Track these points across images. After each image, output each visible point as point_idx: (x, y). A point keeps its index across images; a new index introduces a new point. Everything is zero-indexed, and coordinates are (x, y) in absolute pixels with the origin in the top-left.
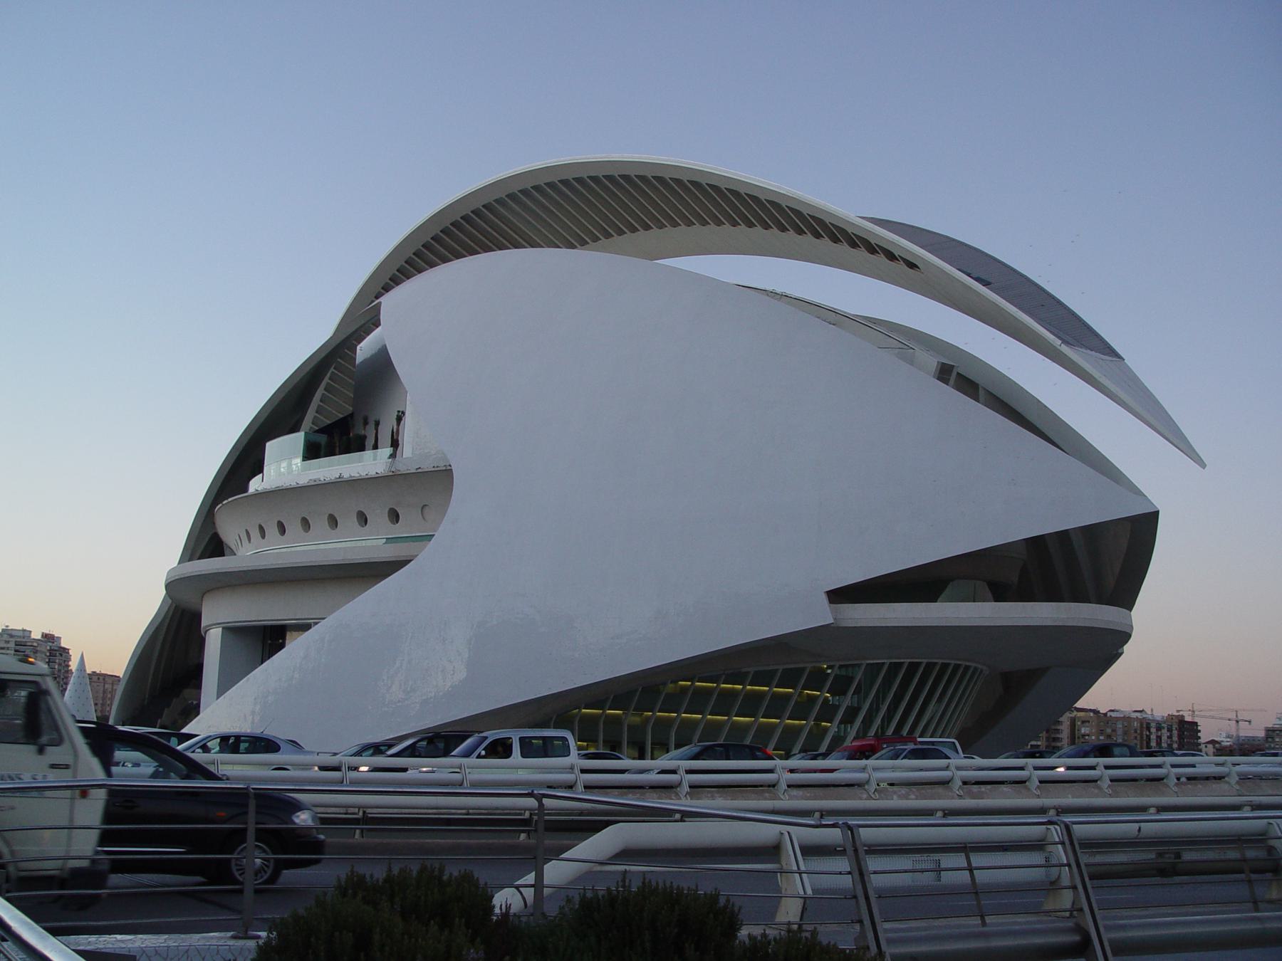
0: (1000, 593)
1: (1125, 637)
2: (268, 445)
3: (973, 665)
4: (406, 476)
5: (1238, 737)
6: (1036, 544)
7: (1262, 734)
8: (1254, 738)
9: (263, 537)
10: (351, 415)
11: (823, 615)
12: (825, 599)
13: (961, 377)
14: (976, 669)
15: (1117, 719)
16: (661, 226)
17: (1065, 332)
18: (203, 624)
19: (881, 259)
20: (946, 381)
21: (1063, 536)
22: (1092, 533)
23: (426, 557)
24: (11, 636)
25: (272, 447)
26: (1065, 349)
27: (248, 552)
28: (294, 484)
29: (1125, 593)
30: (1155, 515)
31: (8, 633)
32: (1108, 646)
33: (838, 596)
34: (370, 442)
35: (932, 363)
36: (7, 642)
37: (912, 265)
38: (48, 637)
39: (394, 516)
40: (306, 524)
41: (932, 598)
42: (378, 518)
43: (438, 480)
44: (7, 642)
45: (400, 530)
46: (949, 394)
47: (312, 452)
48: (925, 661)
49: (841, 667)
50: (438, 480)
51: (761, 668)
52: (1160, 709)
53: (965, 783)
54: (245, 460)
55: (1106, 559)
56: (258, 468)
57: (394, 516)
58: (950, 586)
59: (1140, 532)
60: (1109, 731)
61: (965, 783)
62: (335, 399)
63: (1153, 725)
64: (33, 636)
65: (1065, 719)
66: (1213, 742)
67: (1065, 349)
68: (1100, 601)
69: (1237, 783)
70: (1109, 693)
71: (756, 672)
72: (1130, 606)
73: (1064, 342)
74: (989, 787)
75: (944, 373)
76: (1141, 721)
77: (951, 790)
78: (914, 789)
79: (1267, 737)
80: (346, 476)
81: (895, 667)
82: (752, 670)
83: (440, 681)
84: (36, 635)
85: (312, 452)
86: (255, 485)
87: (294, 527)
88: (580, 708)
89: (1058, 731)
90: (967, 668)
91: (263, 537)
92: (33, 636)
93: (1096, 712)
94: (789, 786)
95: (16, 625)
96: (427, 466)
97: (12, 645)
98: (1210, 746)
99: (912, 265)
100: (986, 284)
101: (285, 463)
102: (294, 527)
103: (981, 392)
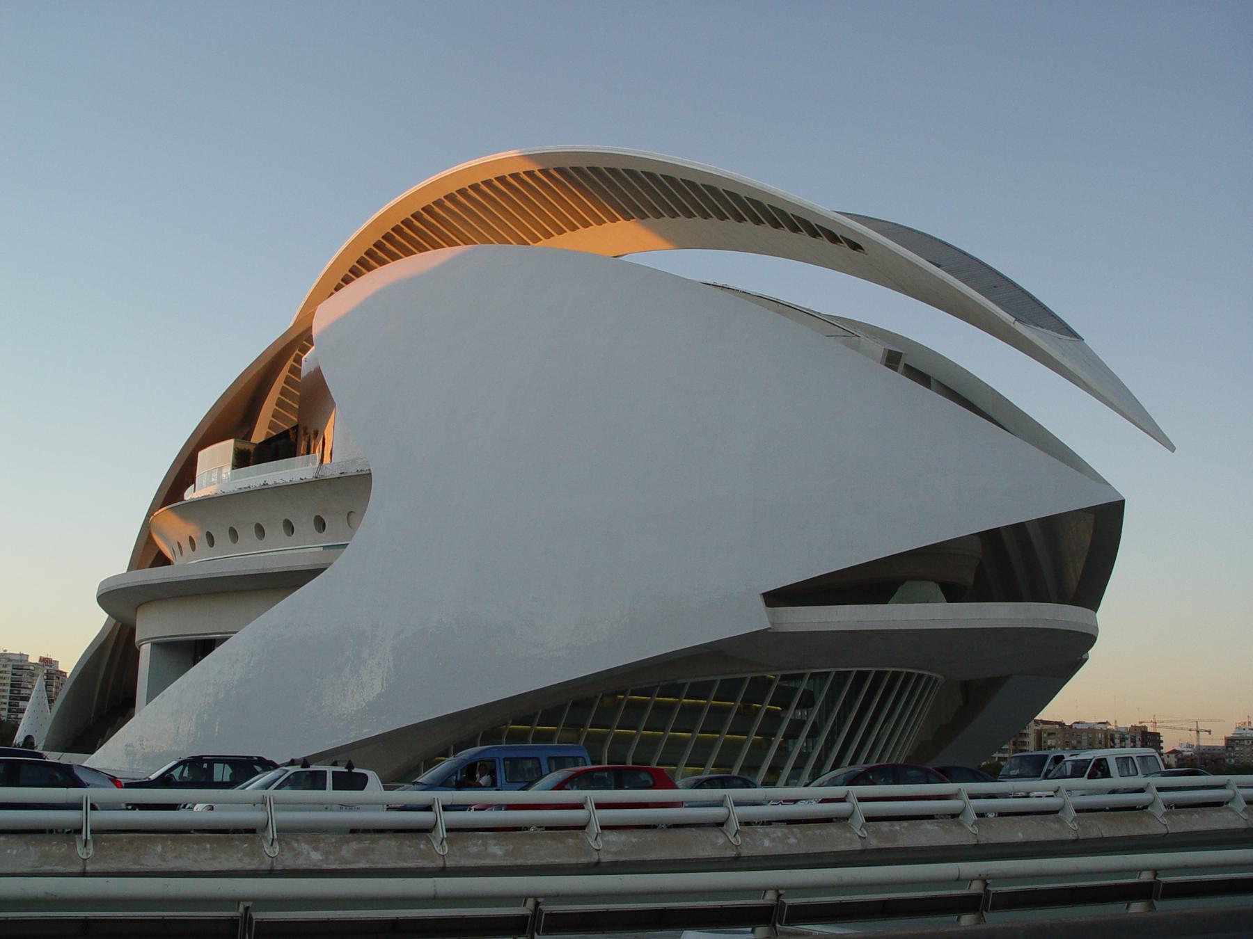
0: (953, 593)
1: (1088, 640)
2: (200, 454)
3: (905, 670)
4: (330, 482)
5: (1199, 746)
6: (991, 538)
7: (1223, 744)
8: (1214, 748)
9: (194, 549)
10: (296, 428)
11: (758, 619)
12: (761, 602)
13: (906, 363)
14: (930, 678)
15: (1082, 730)
16: (600, 222)
17: (1016, 313)
18: (137, 639)
19: (824, 242)
20: (895, 369)
21: (1019, 528)
22: (1050, 525)
23: (341, 564)
24: (9, 660)
25: (203, 455)
26: (1019, 327)
27: (191, 563)
28: (220, 493)
29: (1090, 591)
30: (1122, 503)
31: (5, 657)
32: (1070, 652)
33: (776, 598)
34: (303, 446)
35: (879, 349)
36: (5, 666)
37: (855, 246)
38: (46, 661)
39: (320, 524)
40: (234, 534)
41: (884, 599)
42: (305, 526)
43: (355, 486)
44: (5, 666)
45: (327, 538)
46: (898, 379)
47: (242, 460)
48: (874, 669)
49: (784, 678)
50: (355, 486)
51: (696, 680)
52: (1123, 720)
53: (868, 819)
54: (184, 473)
55: (1068, 554)
56: (192, 480)
57: (320, 524)
58: (900, 589)
59: (1107, 520)
60: (1074, 742)
61: (868, 819)
62: (270, 411)
63: (1139, 743)
64: (30, 660)
65: (1031, 729)
66: (1174, 752)
67: (1019, 327)
68: (1062, 600)
69: (1245, 810)
70: (1070, 705)
71: (692, 685)
72: (1094, 606)
73: (1017, 319)
74: (905, 824)
75: (892, 360)
76: (1106, 732)
77: (850, 829)
78: (796, 829)
79: (1227, 746)
80: (270, 482)
81: (862, 676)
82: (689, 681)
83: (363, 701)
84: (34, 659)
85: (242, 460)
86: (190, 495)
87: (275, 531)
88: (506, 724)
89: (1024, 743)
90: (909, 675)
91: (194, 549)
92: (30, 660)
93: (1061, 724)
94: (603, 828)
95: (14, 649)
96: (352, 471)
97: (9, 669)
98: (1172, 756)
99: (855, 246)
100: (939, 266)
101: (216, 472)
102: (222, 538)
103: (932, 382)
